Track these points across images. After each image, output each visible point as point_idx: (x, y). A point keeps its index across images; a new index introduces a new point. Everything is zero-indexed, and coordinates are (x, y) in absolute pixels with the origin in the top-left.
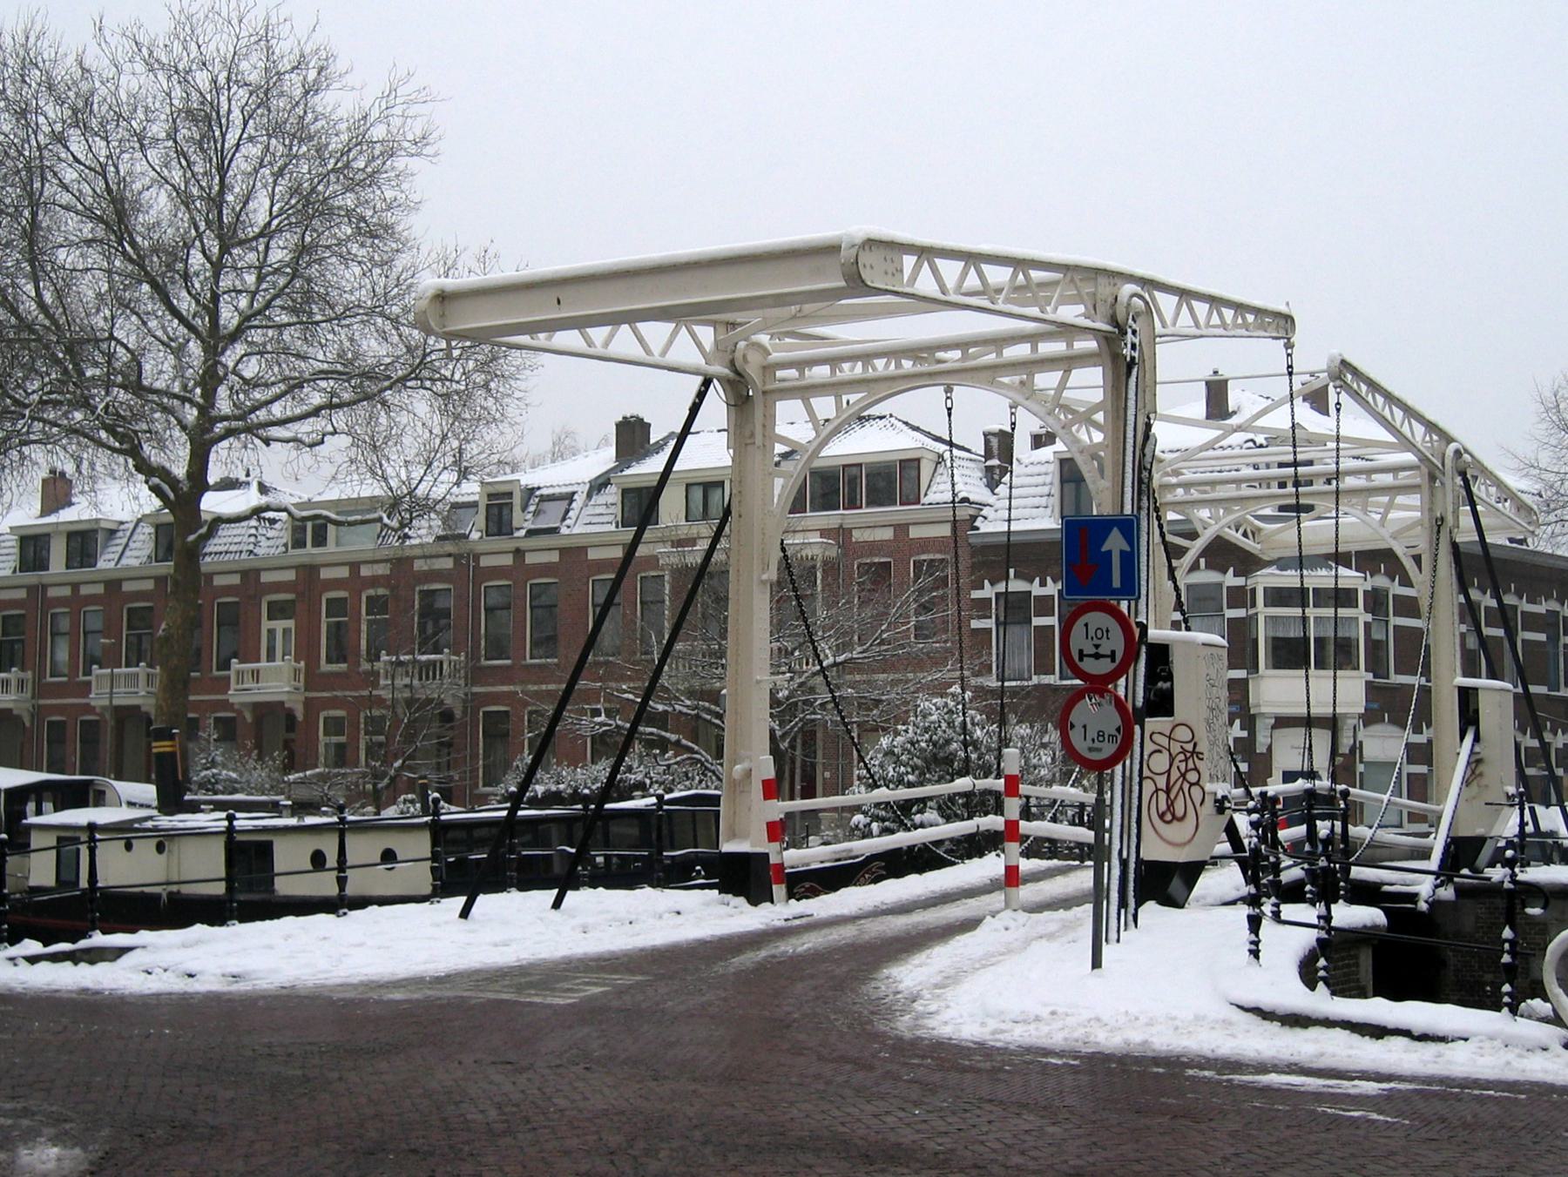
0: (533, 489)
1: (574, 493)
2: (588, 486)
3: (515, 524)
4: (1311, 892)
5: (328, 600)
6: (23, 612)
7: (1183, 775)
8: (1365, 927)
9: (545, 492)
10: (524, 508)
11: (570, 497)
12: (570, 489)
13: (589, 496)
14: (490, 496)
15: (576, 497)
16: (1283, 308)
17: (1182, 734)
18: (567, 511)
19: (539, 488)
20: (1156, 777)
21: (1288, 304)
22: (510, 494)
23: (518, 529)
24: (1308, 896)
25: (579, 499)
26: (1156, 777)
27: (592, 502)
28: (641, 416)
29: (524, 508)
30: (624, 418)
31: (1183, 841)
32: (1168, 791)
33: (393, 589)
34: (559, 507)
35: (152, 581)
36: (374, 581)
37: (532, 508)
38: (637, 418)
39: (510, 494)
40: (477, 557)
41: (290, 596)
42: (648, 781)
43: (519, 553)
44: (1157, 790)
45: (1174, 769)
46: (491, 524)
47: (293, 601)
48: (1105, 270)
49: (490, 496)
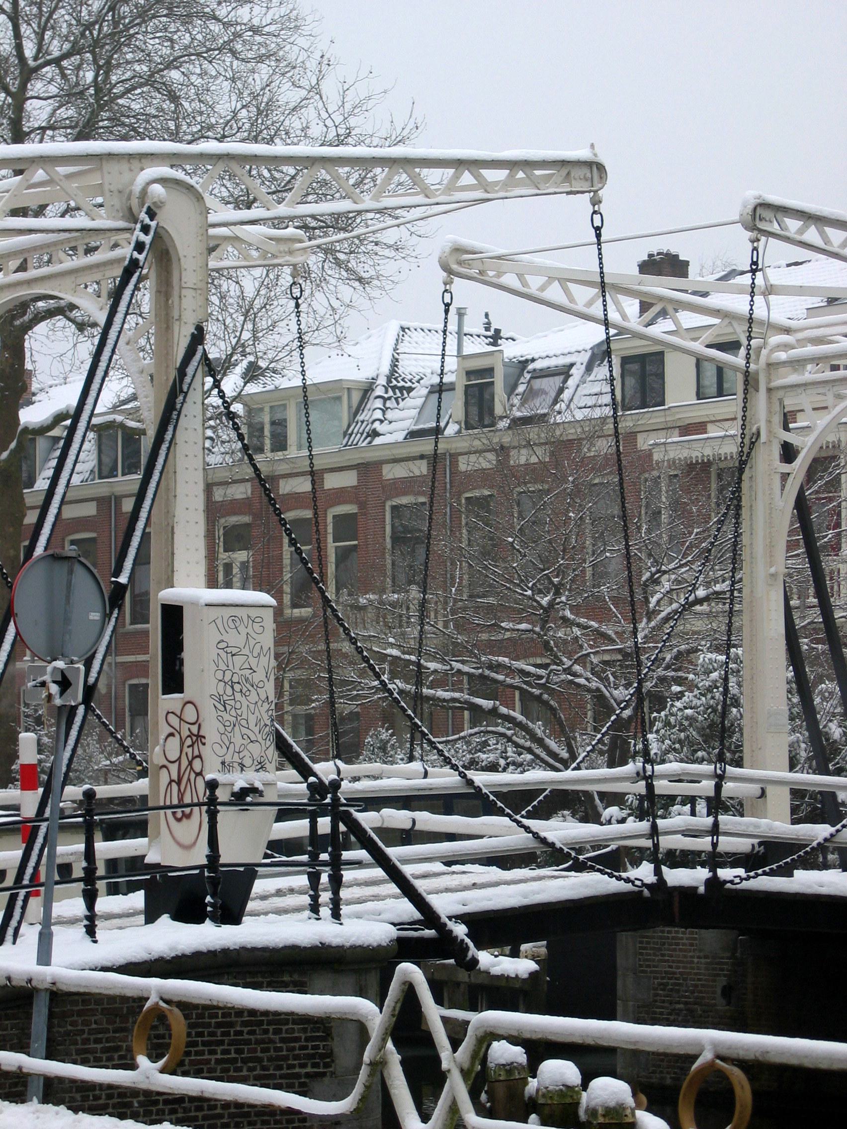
0: (527, 361)
1: (572, 365)
2: (589, 354)
3: (498, 410)
4: (212, 905)
5: (334, 517)
6: (92, 535)
7: (190, 763)
8: (379, 946)
9: (538, 365)
10: (511, 389)
11: (565, 372)
12: (567, 360)
13: (589, 368)
14: (469, 374)
15: (573, 371)
16: (583, 153)
17: (190, 714)
18: (561, 391)
19: (533, 360)
20: (170, 766)
21: (592, 146)
22: (490, 371)
23: (501, 418)
24: (209, 909)
25: (577, 373)
26: (166, 763)
27: (592, 378)
28: (673, 251)
29: (511, 389)
30: (650, 256)
31: (193, 841)
32: (179, 783)
33: (362, 505)
34: (550, 385)
35: (94, 504)
36: (340, 496)
37: (521, 389)
38: (668, 255)
39: (490, 371)
40: (454, 457)
41: (246, 519)
42: (502, 762)
43: (503, 450)
44: (172, 781)
45: (184, 757)
46: (471, 409)
47: (247, 525)
48: (42, 157)
49: (469, 374)
